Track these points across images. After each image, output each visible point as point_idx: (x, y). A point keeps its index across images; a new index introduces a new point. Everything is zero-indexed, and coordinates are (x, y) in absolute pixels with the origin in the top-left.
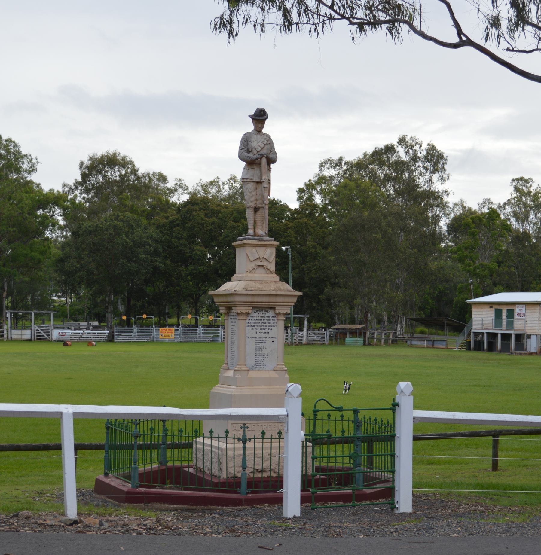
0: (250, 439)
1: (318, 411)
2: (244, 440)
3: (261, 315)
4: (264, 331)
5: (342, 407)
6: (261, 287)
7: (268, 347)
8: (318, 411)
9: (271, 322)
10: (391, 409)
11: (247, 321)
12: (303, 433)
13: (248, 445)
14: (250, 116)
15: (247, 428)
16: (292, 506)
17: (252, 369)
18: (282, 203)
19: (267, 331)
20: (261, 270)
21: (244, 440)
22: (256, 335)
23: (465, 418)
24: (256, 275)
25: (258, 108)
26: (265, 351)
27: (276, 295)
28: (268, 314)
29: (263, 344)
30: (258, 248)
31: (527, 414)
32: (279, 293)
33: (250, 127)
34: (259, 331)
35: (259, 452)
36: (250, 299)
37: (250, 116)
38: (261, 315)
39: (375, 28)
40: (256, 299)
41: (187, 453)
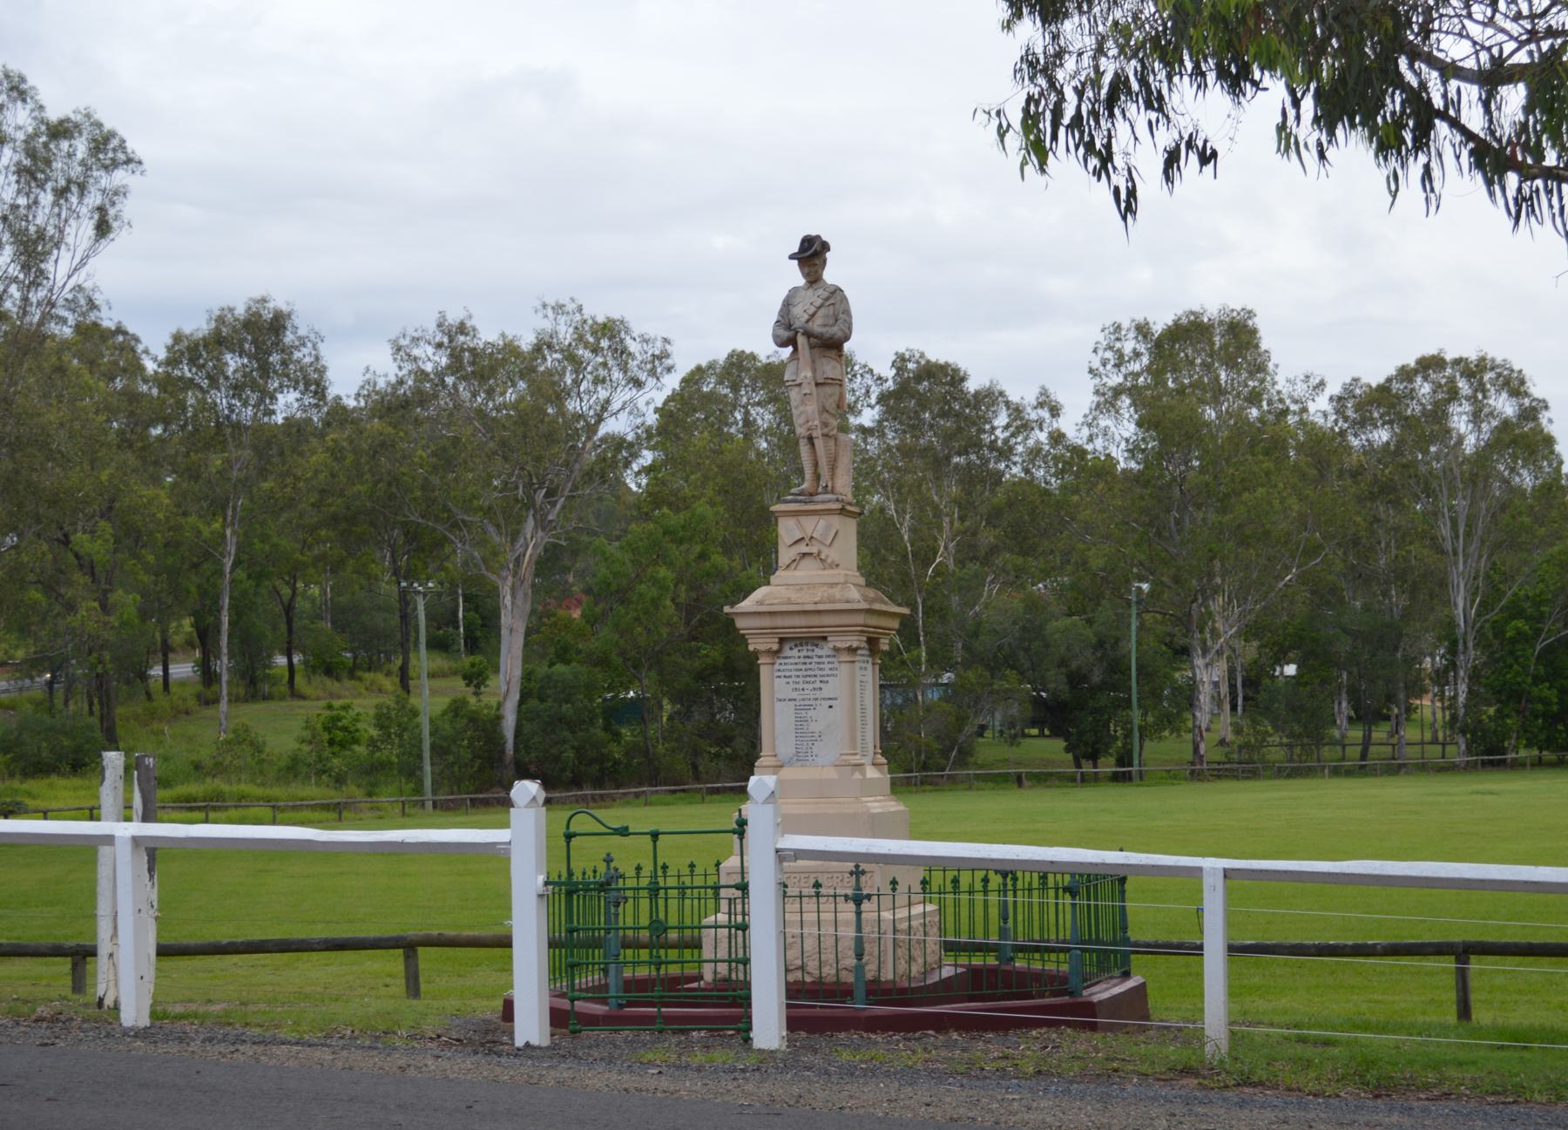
0: (869, 897)
1: (575, 835)
2: (858, 900)
3: (804, 653)
4: (811, 686)
5: (626, 828)
6: (794, 596)
7: (821, 718)
8: (575, 835)
9: (826, 666)
10: (734, 832)
11: (777, 667)
12: (541, 878)
13: (865, 906)
14: (792, 257)
15: (863, 872)
16: (768, 1024)
17: (790, 763)
18: (356, 368)
19: (818, 685)
20: (807, 562)
21: (858, 900)
22: (794, 695)
23: (1333, 870)
24: (797, 573)
25: (1251, 314)
26: (814, 727)
27: (819, 612)
28: (818, 651)
29: (811, 713)
30: (803, 519)
31: (1203, 856)
32: (821, 607)
33: (794, 276)
34: (800, 686)
35: (887, 927)
36: (767, 622)
37: (792, 257)
38: (804, 653)
39: (1386, 159)
40: (779, 622)
41: (964, 927)
